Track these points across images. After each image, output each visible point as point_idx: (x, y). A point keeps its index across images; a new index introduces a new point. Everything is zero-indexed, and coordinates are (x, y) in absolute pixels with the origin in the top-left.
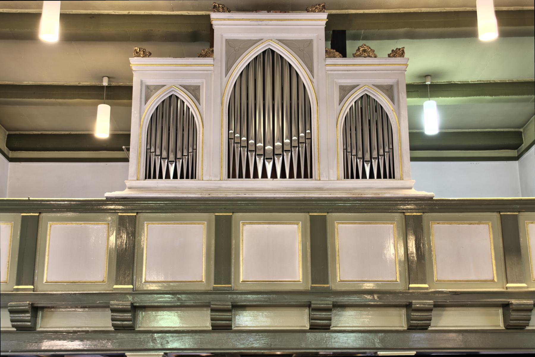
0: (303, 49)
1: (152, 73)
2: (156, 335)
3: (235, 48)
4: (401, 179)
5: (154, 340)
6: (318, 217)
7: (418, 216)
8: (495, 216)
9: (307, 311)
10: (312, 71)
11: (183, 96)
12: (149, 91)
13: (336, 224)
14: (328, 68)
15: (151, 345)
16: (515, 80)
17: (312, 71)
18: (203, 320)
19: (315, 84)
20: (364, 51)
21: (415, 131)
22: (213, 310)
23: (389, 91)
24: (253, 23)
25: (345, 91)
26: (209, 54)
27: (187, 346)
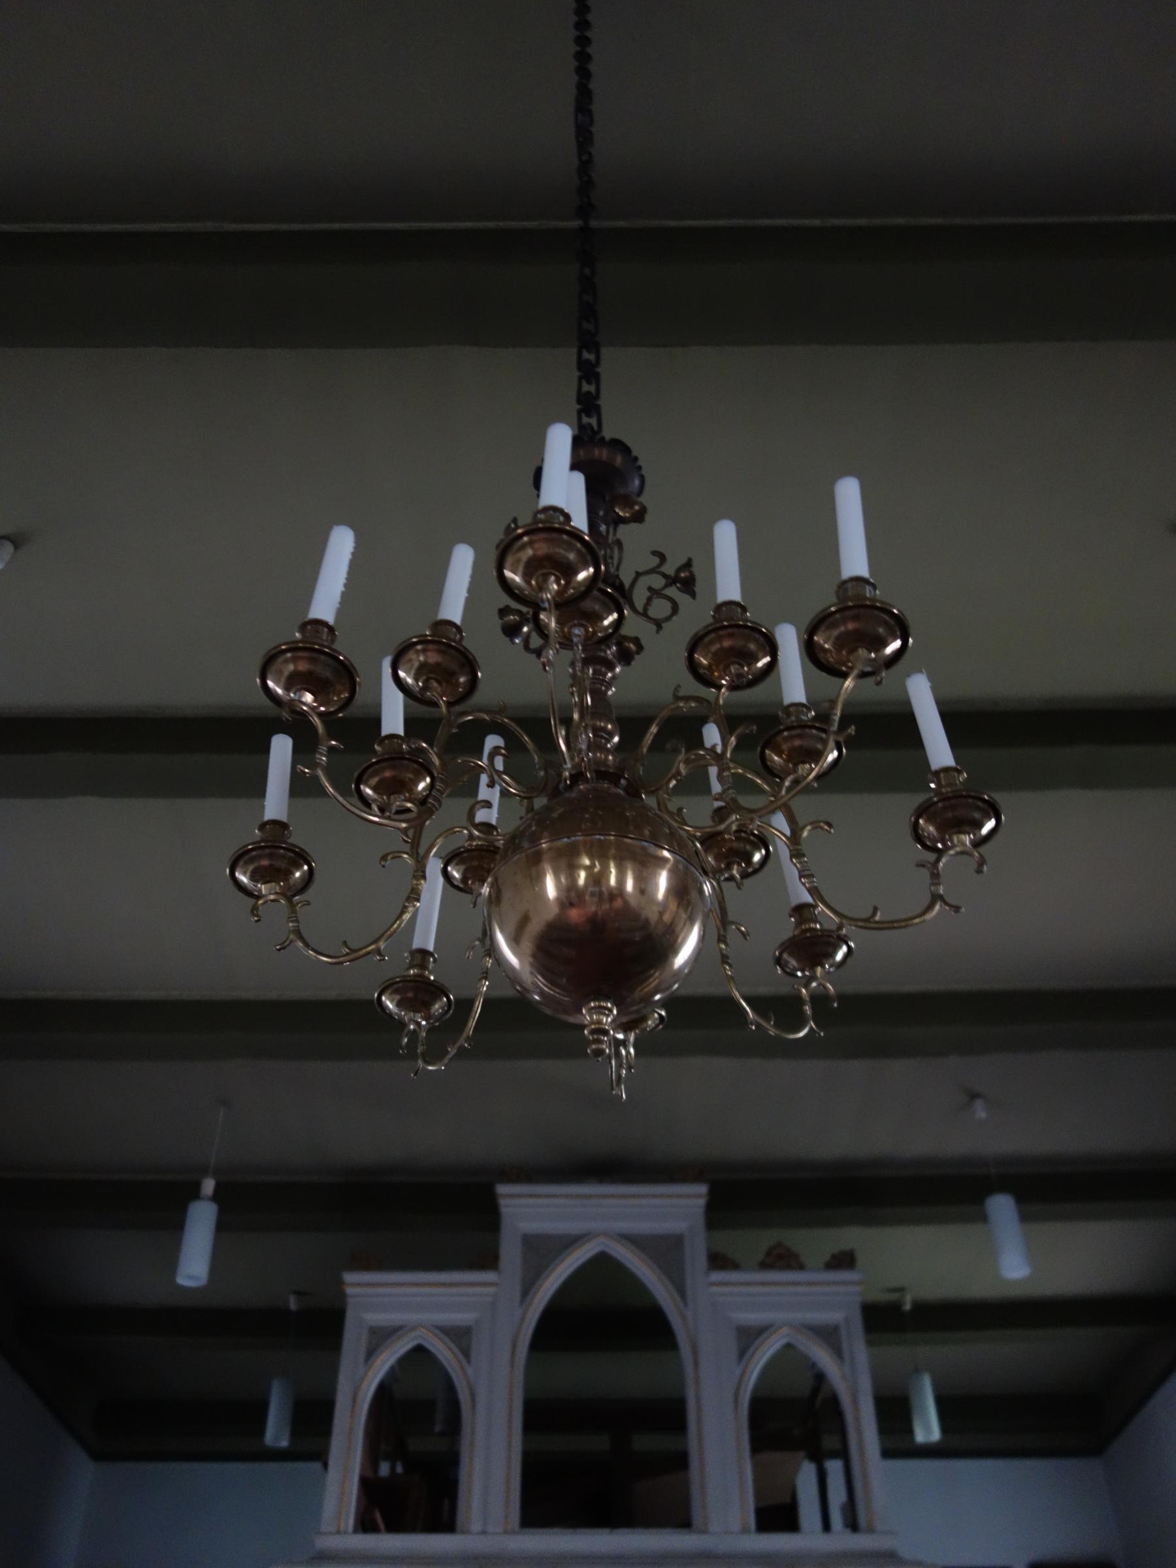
0: (665, 1250)
1: (397, 1309)
3: (542, 1250)
10: (682, 1293)
12: (380, 1337)
14: (714, 1289)
17: (682, 1293)
20: (780, 1257)
23: (829, 1335)
25: (748, 1337)
26: (488, 1260)
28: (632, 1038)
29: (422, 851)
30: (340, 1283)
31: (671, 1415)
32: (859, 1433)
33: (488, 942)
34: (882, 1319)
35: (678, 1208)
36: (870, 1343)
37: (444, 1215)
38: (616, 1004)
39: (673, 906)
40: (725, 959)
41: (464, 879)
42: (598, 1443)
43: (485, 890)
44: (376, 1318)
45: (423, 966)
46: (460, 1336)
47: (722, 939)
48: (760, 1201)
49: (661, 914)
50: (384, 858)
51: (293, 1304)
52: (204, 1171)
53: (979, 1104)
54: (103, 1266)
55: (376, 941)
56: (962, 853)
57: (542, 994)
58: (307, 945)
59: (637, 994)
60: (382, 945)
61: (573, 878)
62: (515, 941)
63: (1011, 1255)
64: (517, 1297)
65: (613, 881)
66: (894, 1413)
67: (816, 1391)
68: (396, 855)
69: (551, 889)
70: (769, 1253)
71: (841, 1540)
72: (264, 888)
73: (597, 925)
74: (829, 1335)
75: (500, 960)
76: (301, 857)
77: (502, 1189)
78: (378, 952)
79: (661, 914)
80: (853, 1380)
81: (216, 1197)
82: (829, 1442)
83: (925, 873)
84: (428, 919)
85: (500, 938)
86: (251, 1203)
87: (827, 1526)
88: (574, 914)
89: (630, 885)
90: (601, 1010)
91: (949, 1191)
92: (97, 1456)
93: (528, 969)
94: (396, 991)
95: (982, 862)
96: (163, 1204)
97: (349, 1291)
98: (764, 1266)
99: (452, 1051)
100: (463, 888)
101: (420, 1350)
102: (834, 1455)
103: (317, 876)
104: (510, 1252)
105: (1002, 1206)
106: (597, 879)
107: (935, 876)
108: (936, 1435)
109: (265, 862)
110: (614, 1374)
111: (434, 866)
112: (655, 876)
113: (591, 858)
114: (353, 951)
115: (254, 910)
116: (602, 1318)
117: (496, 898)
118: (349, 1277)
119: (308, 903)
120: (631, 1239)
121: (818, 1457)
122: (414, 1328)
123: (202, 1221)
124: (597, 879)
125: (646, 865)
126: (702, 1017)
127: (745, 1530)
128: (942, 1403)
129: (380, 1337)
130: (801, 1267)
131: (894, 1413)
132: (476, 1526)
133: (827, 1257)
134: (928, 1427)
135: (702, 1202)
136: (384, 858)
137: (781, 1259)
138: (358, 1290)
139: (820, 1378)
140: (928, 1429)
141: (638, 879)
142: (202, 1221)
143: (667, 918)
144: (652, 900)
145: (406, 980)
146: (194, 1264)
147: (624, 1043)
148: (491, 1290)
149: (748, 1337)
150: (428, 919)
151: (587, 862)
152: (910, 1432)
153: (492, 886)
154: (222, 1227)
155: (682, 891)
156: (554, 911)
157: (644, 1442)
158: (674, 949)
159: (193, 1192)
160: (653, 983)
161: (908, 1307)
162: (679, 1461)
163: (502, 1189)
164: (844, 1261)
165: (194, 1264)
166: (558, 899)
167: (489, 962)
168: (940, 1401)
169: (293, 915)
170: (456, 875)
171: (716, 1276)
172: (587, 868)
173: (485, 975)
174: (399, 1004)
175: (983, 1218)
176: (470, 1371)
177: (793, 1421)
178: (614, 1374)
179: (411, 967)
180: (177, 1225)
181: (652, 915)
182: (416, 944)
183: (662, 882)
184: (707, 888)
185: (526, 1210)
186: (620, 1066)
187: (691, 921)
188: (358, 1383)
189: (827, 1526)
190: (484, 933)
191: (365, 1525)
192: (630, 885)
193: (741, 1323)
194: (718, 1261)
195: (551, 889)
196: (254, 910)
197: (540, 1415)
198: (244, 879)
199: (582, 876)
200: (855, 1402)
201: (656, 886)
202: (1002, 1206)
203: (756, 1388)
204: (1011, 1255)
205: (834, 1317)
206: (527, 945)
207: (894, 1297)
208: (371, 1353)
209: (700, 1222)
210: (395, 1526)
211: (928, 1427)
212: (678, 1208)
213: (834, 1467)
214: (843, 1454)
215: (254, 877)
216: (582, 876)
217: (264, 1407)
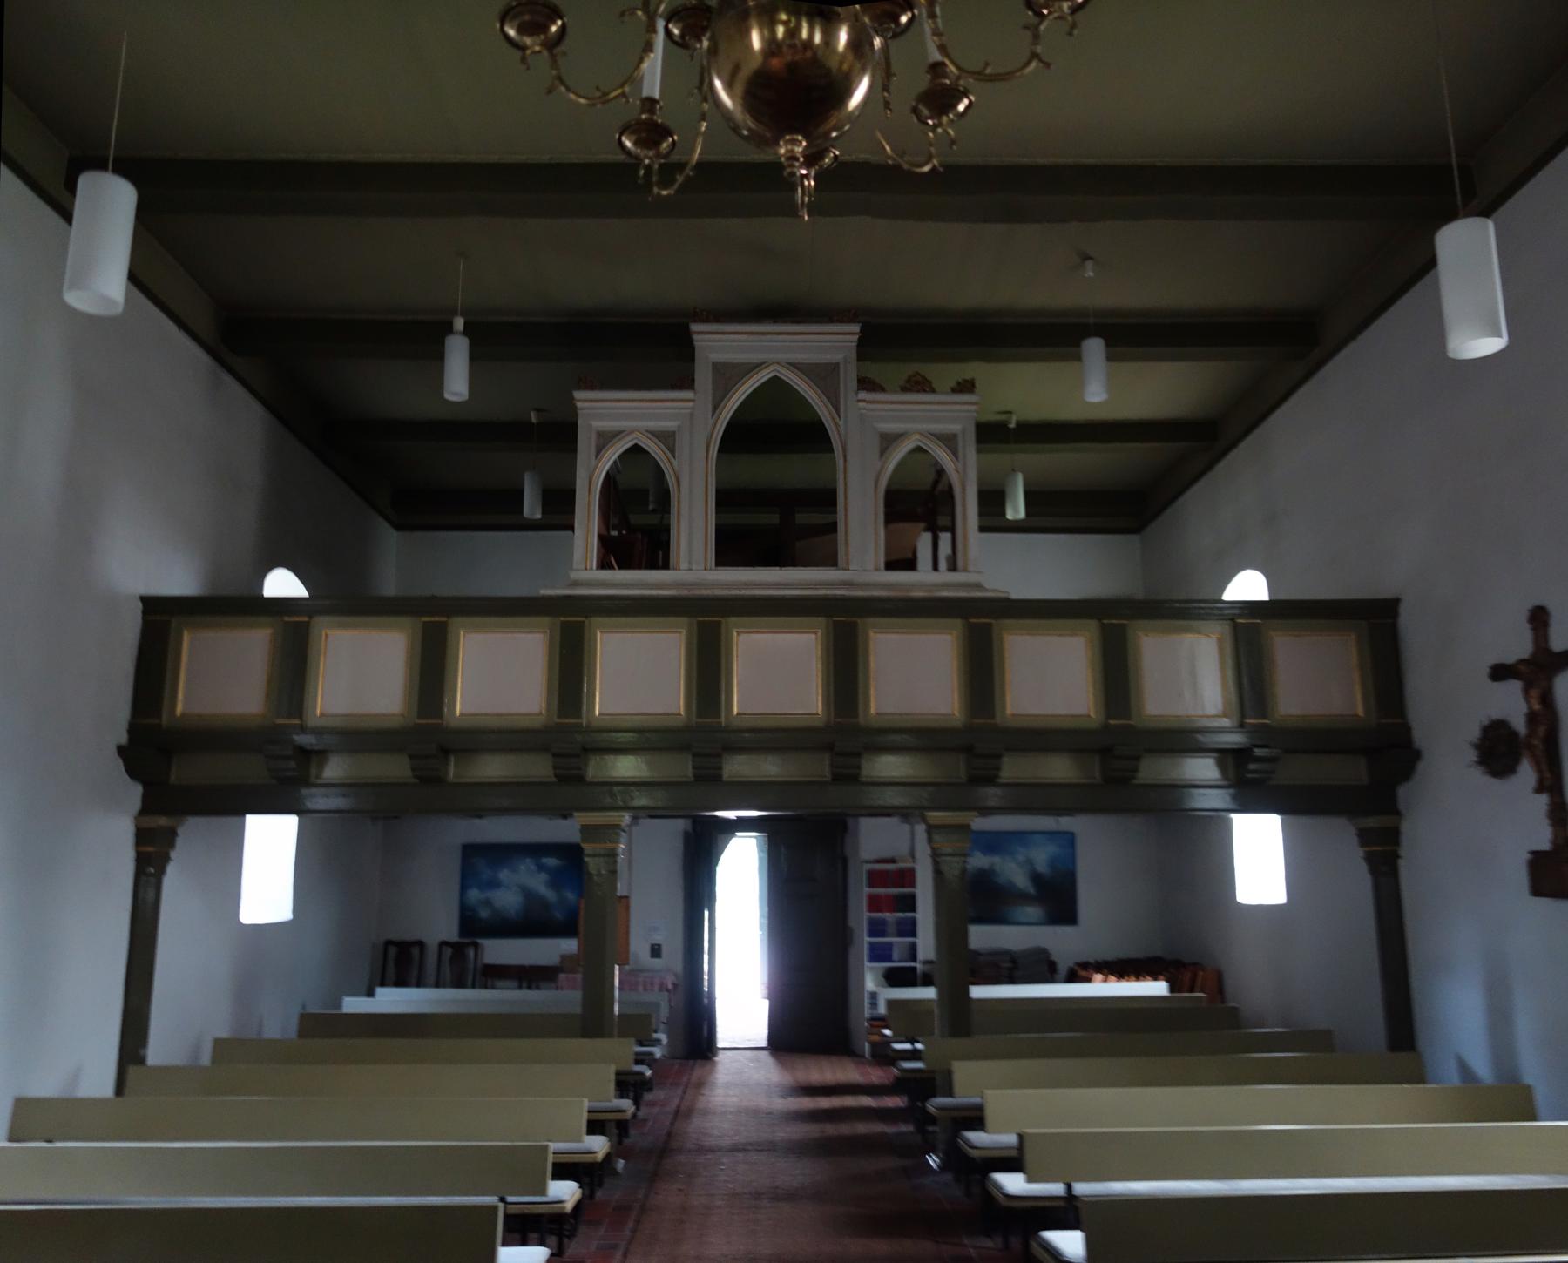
0: (824, 375)
1: (615, 419)
2: (615, 789)
3: (727, 376)
4: (965, 570)
5: (612, 795)
6: (845, 626)
7: (982, 623)
8: (1093, 625)
9: (827, 757)
10: (837, 410)
11: (654, 448)
12: (605, 440)
13: (872, 634)
14: (861, 405)
15: (608, 800)
16: (1169, 510)
17: (837, 410)
18: (816, 767)
19: (842, 429)
20: (917, 383)
21: (1371, 822)
22: (554, 755)
23: (949, 441)
24: (751, 338)
25: (888, 441)
26: (686, 382)
27: (660, 804)
28: (813, 173)
29: (652, 7)
30: (573, 398)
31: (826, 499)
32: (964, 506)
33: (705, 87)
34: (991, 434)
35: (835, 343)
36: (979, 451)
37: (651, 347)
38: (806, 137)
39: (850, 57)
40: (887, 105)
41: (682, 36)
42: (771, 519)
43: (706, 44)
44: (599, 425)
45: (652, 111)
46: (668, 439)
47: (886, 88)
48: (903, 340)
49: (841, 63)
50: (622, 14)
51: (534, 418)
52: (455, 313)
53: (1089, 264)
54: (384, 388)
55: (622, 86)
56: (1060, 18)
57: (749, 129)
58: (568, 89)
59: (821, 130)
60: (627, 89)
61: (773, 32)
62: (729, 86)
63: (1096, 386)
64: (710, 407)
65: (804, 34)
66: (991, 501)
67: (936, 482)
68: (632, 11)
69: (756, 41)
70: (908, 381)
71: (944, 576)
72: (528, 41)
73: (792, 67)
74: (949, 441)
75: (717, 103)
76: (556, 13)
77: (694, 327)
78: (623, 95)
79: (841, 63)
80: (965, 475)
81: (467, 331)
82: (943, 521)
83: (1028, 34)
84: (653, 74)
85: (718, 84)
86: (490, 339)
87: (936, 568)
88: (775, 63)
89: (818, 38)
90: (795, 142)
91: (1054, 336)
92: (399, 527)
93: (739, 109)
94: (632, 133)
95: (1074, 26)
96: (424, 339)
97: (579, 405)
98: (904, 389)
99: (689, 172)
100: (681, 43)
101: (636, 450)
102: (945, 529)
103: (569, 30)
104: (703, 376)
105: (1094, 348)
106: (793, 33)
107: (1036, 37)
108: (1022, 514)
109: (527, 17)
110: (782, 470)
111: (660, 24)
112: (837, 31)
113: (789, 13)
114: (606, 94)
115: (524, 60)
116: (774, 429)
117: (713, 51)
118: (578, 395)
119: (565, 54)
120: (796, 366)
121: (934, 530)
122: (632, 432)
123: (457, 354)
124: (793, 33)
125: (829, 24)
126: (860, 185)
127: (877, 569)
128: (1029, 495)
129: (605, 440)
130: (933, 391)
131: (991, 501)
132: (684, 565)
133: (953, 384)
134: (1016, 509)
135: (856, 338)
136: (622, 14)
137: (919, 384)
138: (586, 405)
139: (941, 472)
140: (1016, 511)
141: (825, 34)
142: (457, 354)
143: (845, 67)
144: (835, 50)
145: (639, 123)
146: (457, 382)
147: (806, 176)
148: (690, 404)
149: (888, 441)
150: (653, 74)
151: (784, 17)
152: (1004, 514)
153: (710, 39)
154: (473, 358)
155: (858, 44)
156: (759, 60)
157: (803, 518)
158: (849, 93)
159: (448, 329)
160: (833, 121)
161: (1012, 425)
162: (833, 528)
163: (694, 327)
164: (967, 387)
165: (457, 382)
166: (763, 50)
167: (706, 106)
168: (1027, 494)
169: (554, 62)
170: (676, 32)
171: (863, 395)
172: (785, 23)
173: (703, 117)
174: (636, 143)
175: (1078, 358)
176: (675, 463)
177: (918, 505)
178: (782, 470)
179: (643, 112)
180: (439, 356)
181: (833, 64)
182: (645, 93)
183: (843, 37)
184: (877, 42)
185: (716, 344)
186: (803, 194)
187: (863, 71)
188: (591, 473)
189: (936, 568)
190: (702, 82)
191: (604, 565)
192: (818, 38)
193: (881, 431)
194: (865, 384)
195: (756, 41)
196: (524, 60)
197: (726, 499)
198: (512, 33)
199: (780, 30)
200: (964, 489)
201: (838, 39)
202: (1094, 348)
203: (889, 485)
204: (1096, 386)
205: (955, 427)
206: (739, 87)
207: (1003, 417)
208: (599, 451)
209: (854, 355)
210: (624, 565)
211: (1016, 509)
212: (835, 343)
213: (945, 538)
214: (952, 529)
215: (520, 31)
216: (780, 30)
217: (519, 494)
